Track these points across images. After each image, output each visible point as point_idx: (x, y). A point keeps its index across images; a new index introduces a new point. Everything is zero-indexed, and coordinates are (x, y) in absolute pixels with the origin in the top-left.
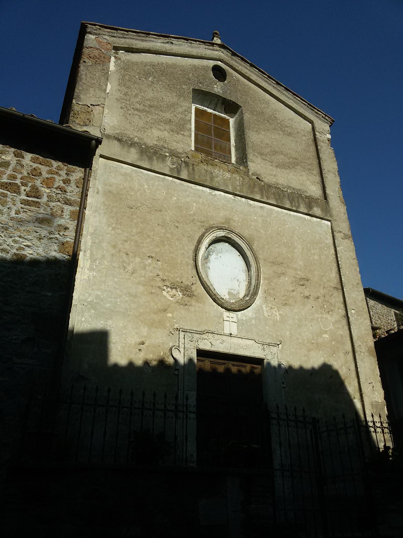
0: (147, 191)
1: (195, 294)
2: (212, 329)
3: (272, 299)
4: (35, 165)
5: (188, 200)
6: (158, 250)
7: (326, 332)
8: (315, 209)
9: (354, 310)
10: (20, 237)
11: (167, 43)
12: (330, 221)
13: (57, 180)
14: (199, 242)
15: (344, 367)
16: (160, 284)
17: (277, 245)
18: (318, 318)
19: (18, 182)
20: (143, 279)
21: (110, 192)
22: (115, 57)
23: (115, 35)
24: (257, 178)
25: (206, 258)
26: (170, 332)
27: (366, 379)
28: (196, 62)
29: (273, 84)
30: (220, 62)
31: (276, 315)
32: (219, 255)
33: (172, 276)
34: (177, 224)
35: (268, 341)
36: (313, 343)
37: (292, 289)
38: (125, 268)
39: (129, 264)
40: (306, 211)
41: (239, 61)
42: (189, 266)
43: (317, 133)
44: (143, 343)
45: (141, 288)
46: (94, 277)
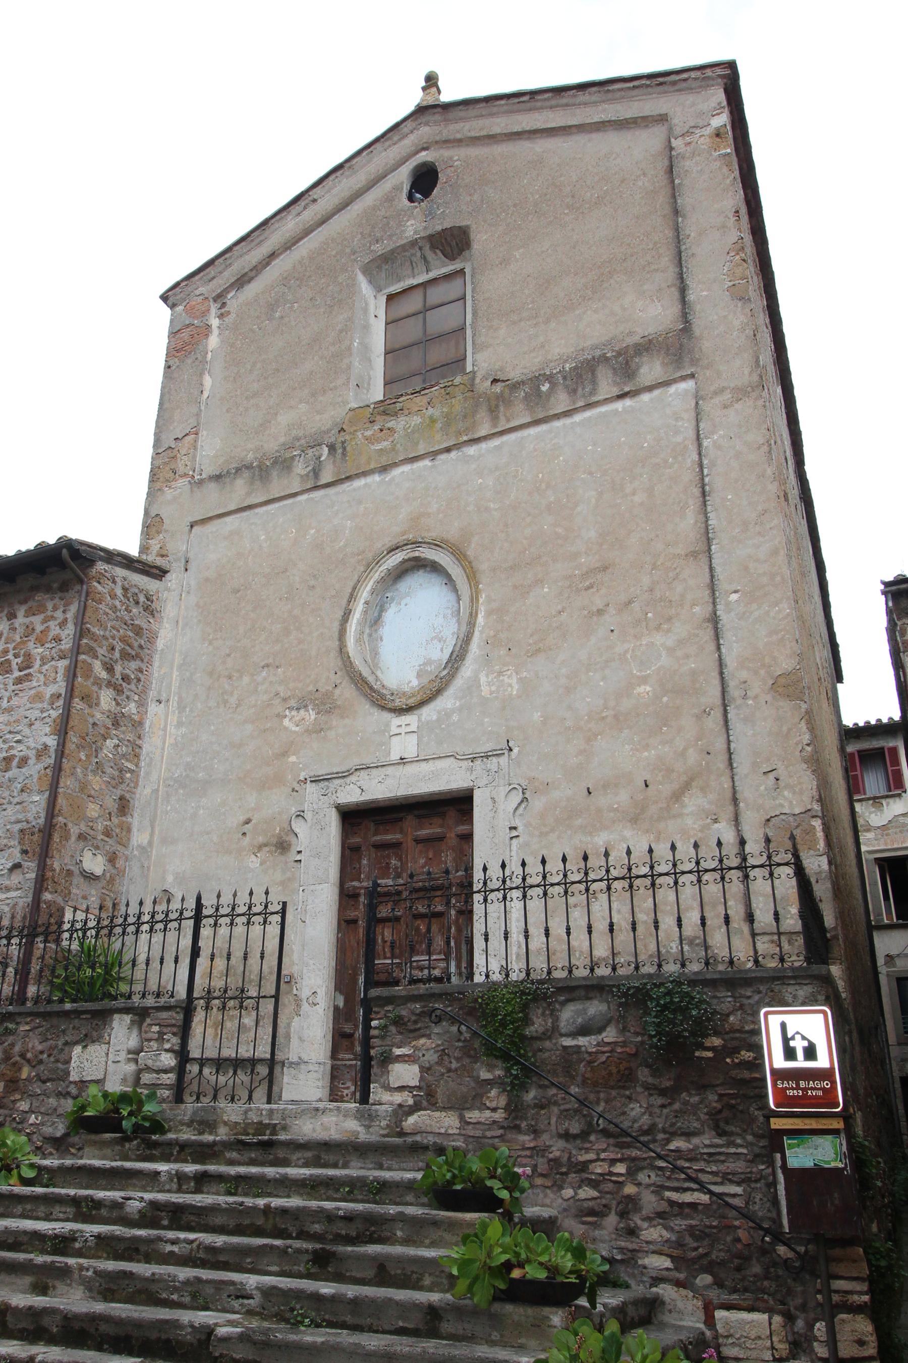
0: (264, 545)
1: (339, 703)
2: (367, 761)
3: (503, 652)
4: (27, 620)
5: (336, 521)
6: (277, 647)
7: (644, 680)
8: (644, 370)
9: (736, 592)
10: (10, 732)
11: (305, 208)
12: (692, 376)
13: (53, 627)
14: (352, 597)
15: (691, 751)
16: (279, 709)
17: (528, 520)
18: (626, 652)
19: (10, 656)
20: (253, 710)
21: (207, 580)
22: (221, 316)
23: (213, 274)
24: (495, 381)
25: (375, 621)
26: (293, 790)
27: (755, 765)
28: (357, 208)
29: (548, 104)
30: (424, 153)
31: (510, 685)
32: (403, 602)
33: (300, 685)
34: (312, 583)
35: (488, 746)
36: (603, 718)
37: (559, 607)
38: (225, 702)
39: (232, 694)
40: (616, 391)
41: (462, 114)
42: (332, 655)
43: (674, 143)
44: (248, 822)
45: (249, 727)
46: (183, 736)
